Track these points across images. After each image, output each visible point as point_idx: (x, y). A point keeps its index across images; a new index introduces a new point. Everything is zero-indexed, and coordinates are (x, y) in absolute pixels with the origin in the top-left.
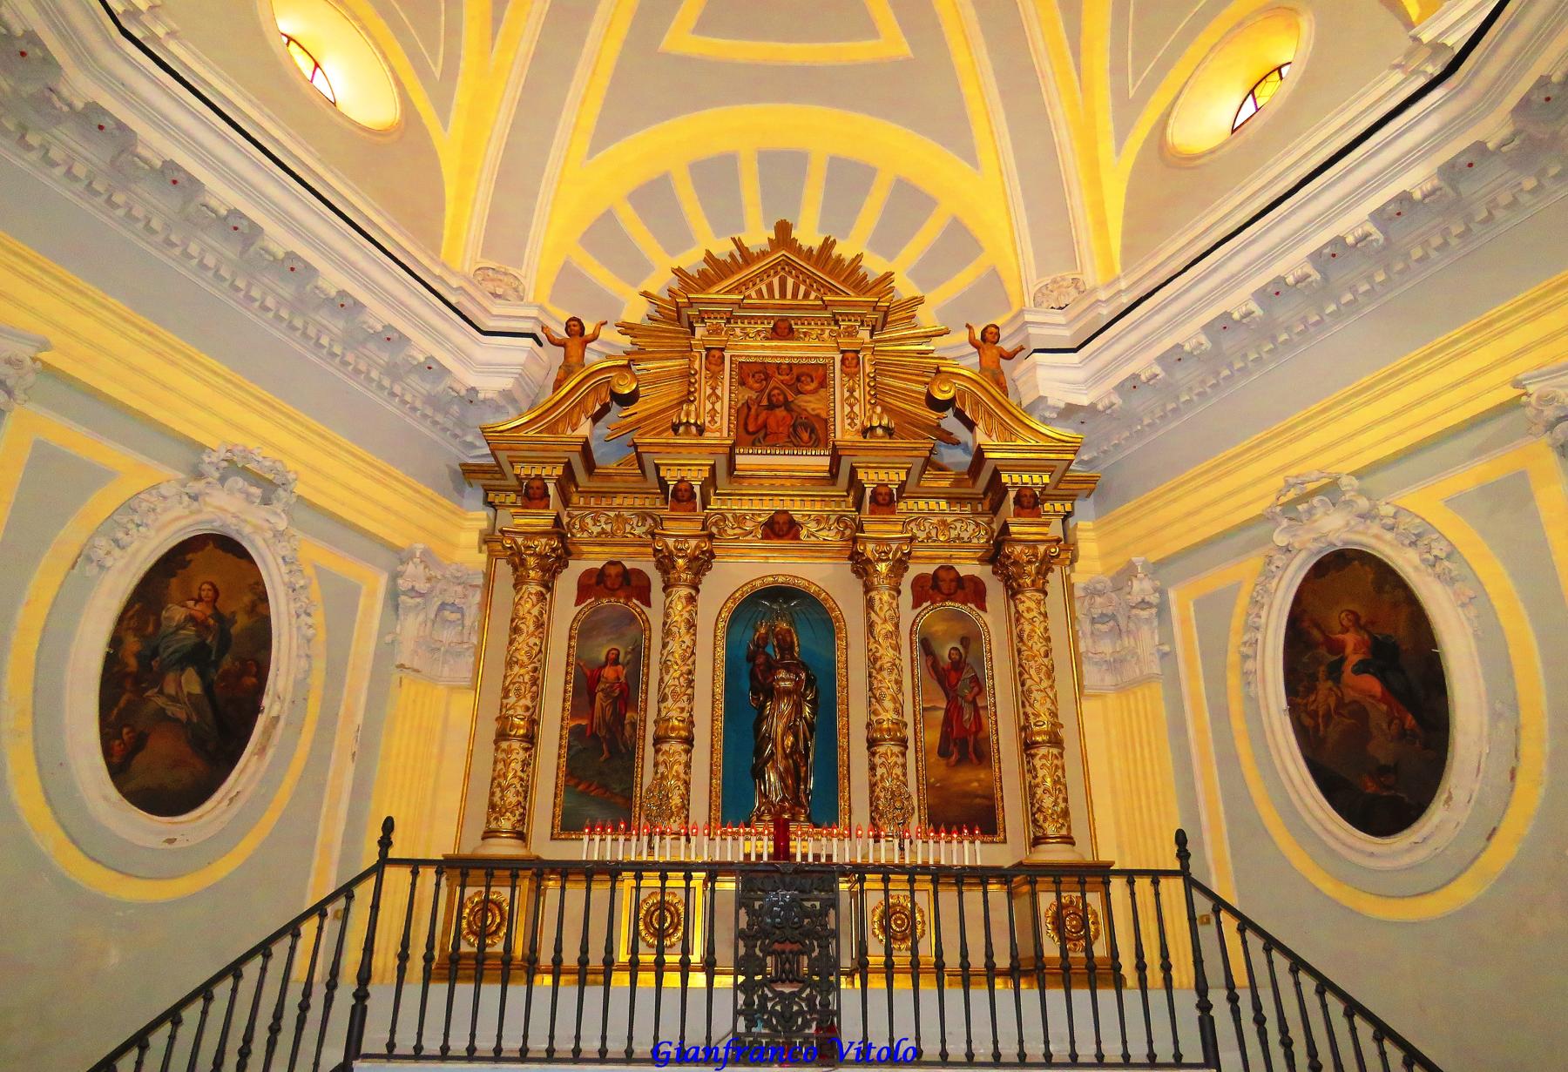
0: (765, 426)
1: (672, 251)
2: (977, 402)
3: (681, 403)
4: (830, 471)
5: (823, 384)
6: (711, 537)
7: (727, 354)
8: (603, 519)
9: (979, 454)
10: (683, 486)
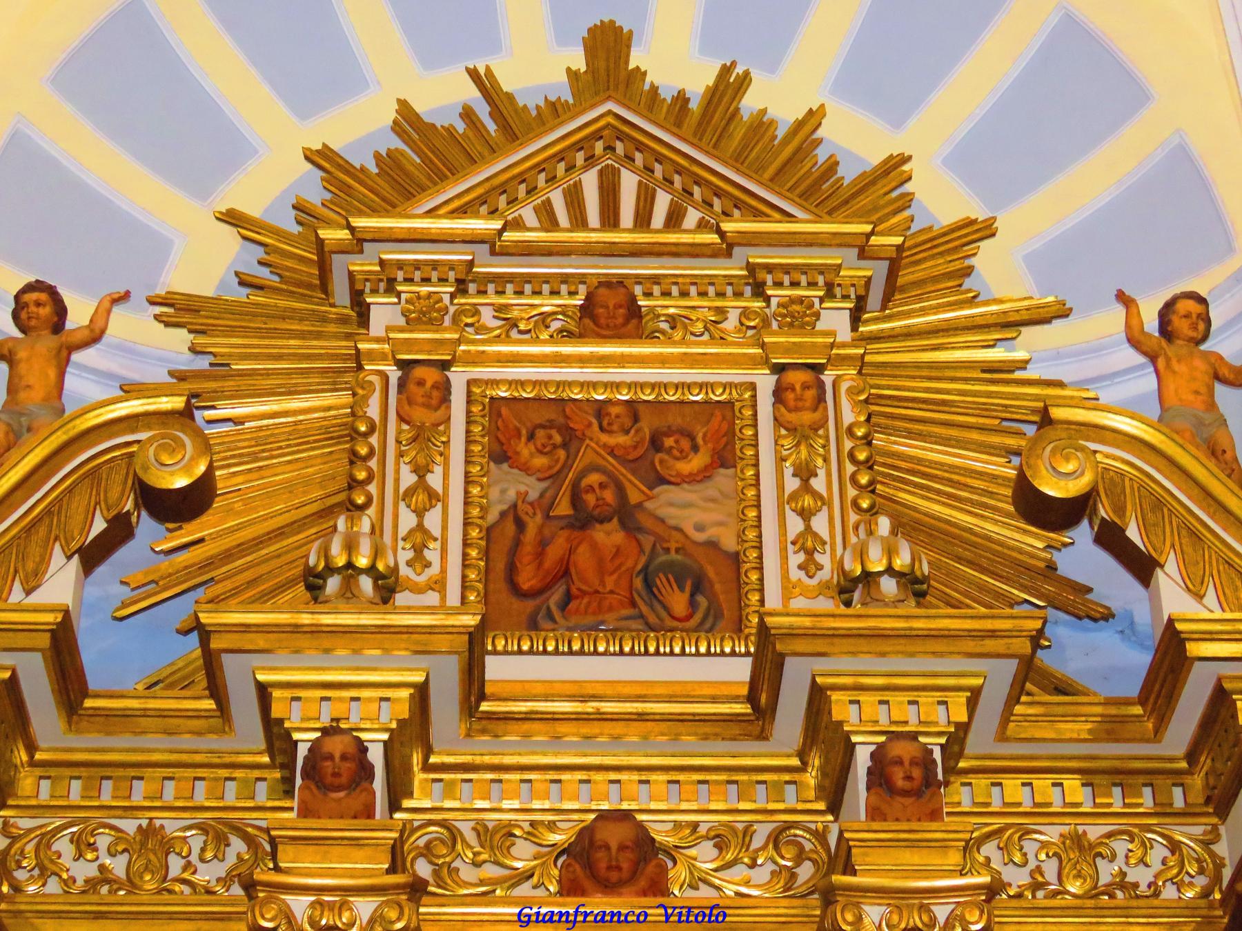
0: (564, 572)
1: (305, 104)
2: (1157, 505)
3: (327, 513)
4: (752, 698)
5: (724, 458)
6: (417, 890)
7: (458, 377)
8: (103, 841)
9: (1171, 654)
10: (336, 746)
